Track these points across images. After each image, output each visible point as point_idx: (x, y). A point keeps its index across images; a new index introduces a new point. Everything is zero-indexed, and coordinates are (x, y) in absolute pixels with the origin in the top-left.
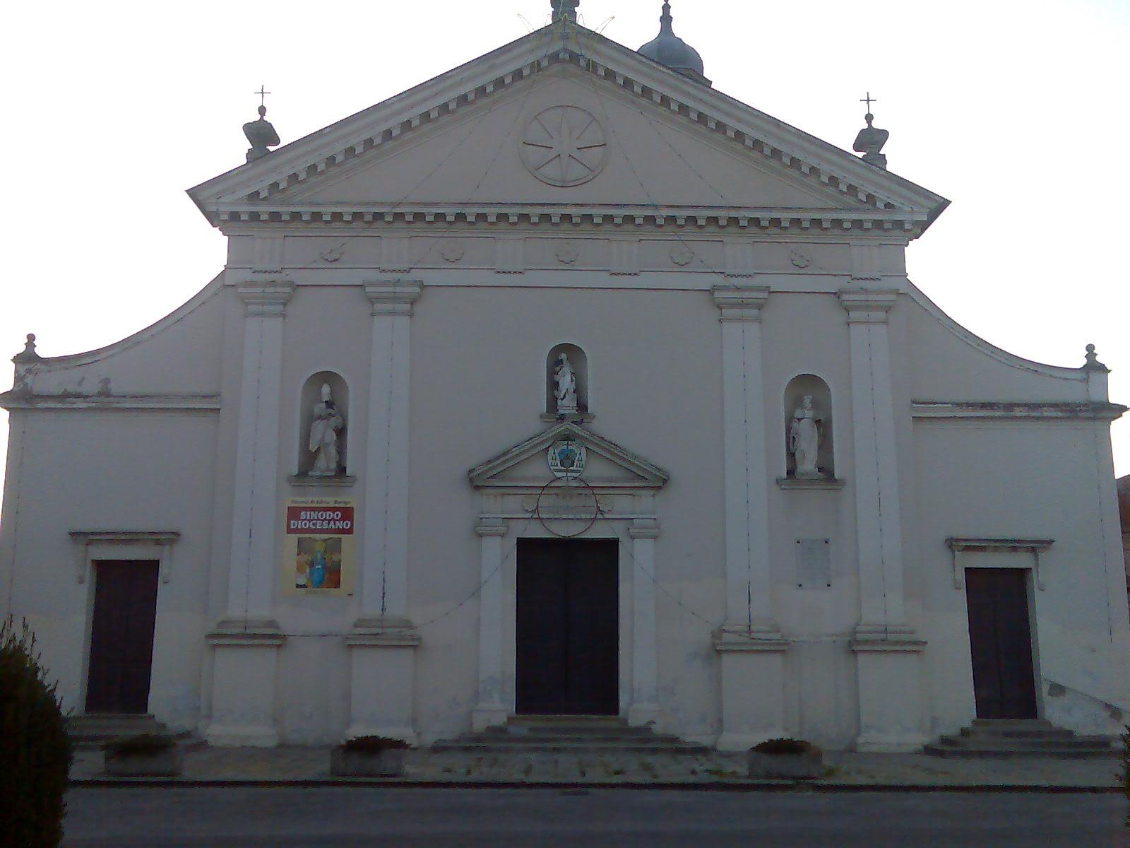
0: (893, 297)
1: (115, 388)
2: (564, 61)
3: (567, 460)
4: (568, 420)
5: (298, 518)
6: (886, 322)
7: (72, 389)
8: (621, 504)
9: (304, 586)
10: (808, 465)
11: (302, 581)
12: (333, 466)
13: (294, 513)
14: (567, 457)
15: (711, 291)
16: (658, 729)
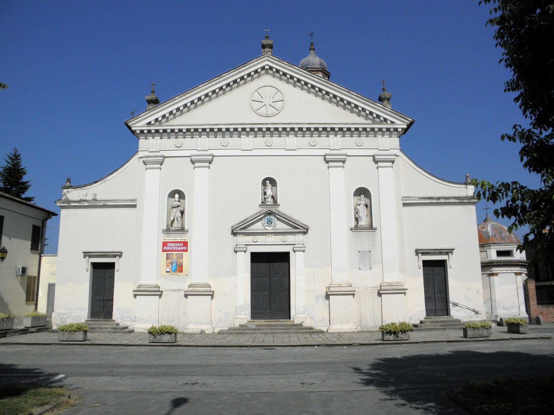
0: (345, 157)
1: (98, 198)
2: (267, 69)
3: (270, 222)
4: (270, 211)
5: (166, 246)
6: (343, 167)
7: (83, 198)
8: (290, 239)
9: (169, 272)
10: (364, 222)
11: (168, 270)
12: (180, 225)
13: (165, 244)
14: (270, 221)
15: (325, 156)
16: (304, 325)
